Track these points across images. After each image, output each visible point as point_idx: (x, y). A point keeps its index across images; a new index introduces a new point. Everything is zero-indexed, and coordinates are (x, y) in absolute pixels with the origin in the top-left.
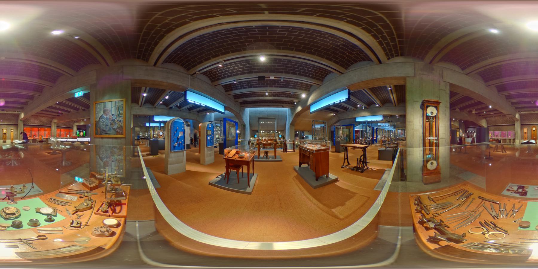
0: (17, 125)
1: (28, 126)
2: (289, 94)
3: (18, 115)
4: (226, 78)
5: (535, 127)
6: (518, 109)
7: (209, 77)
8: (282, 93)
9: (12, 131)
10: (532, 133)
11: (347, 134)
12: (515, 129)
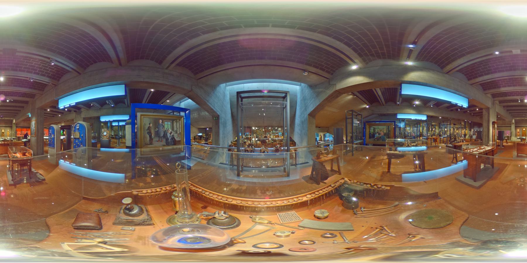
0: (12, 127)
1: (20, 127)
2: (524, 92)
3: (12, 121)
4: (484, 76)
5: (525, 128)
6: (514, 117)
7: (465, 75)
8: (520, 91)
9: (8, 131)
10: (522, 132)
11: (385, 132)
12: (511, 129)
